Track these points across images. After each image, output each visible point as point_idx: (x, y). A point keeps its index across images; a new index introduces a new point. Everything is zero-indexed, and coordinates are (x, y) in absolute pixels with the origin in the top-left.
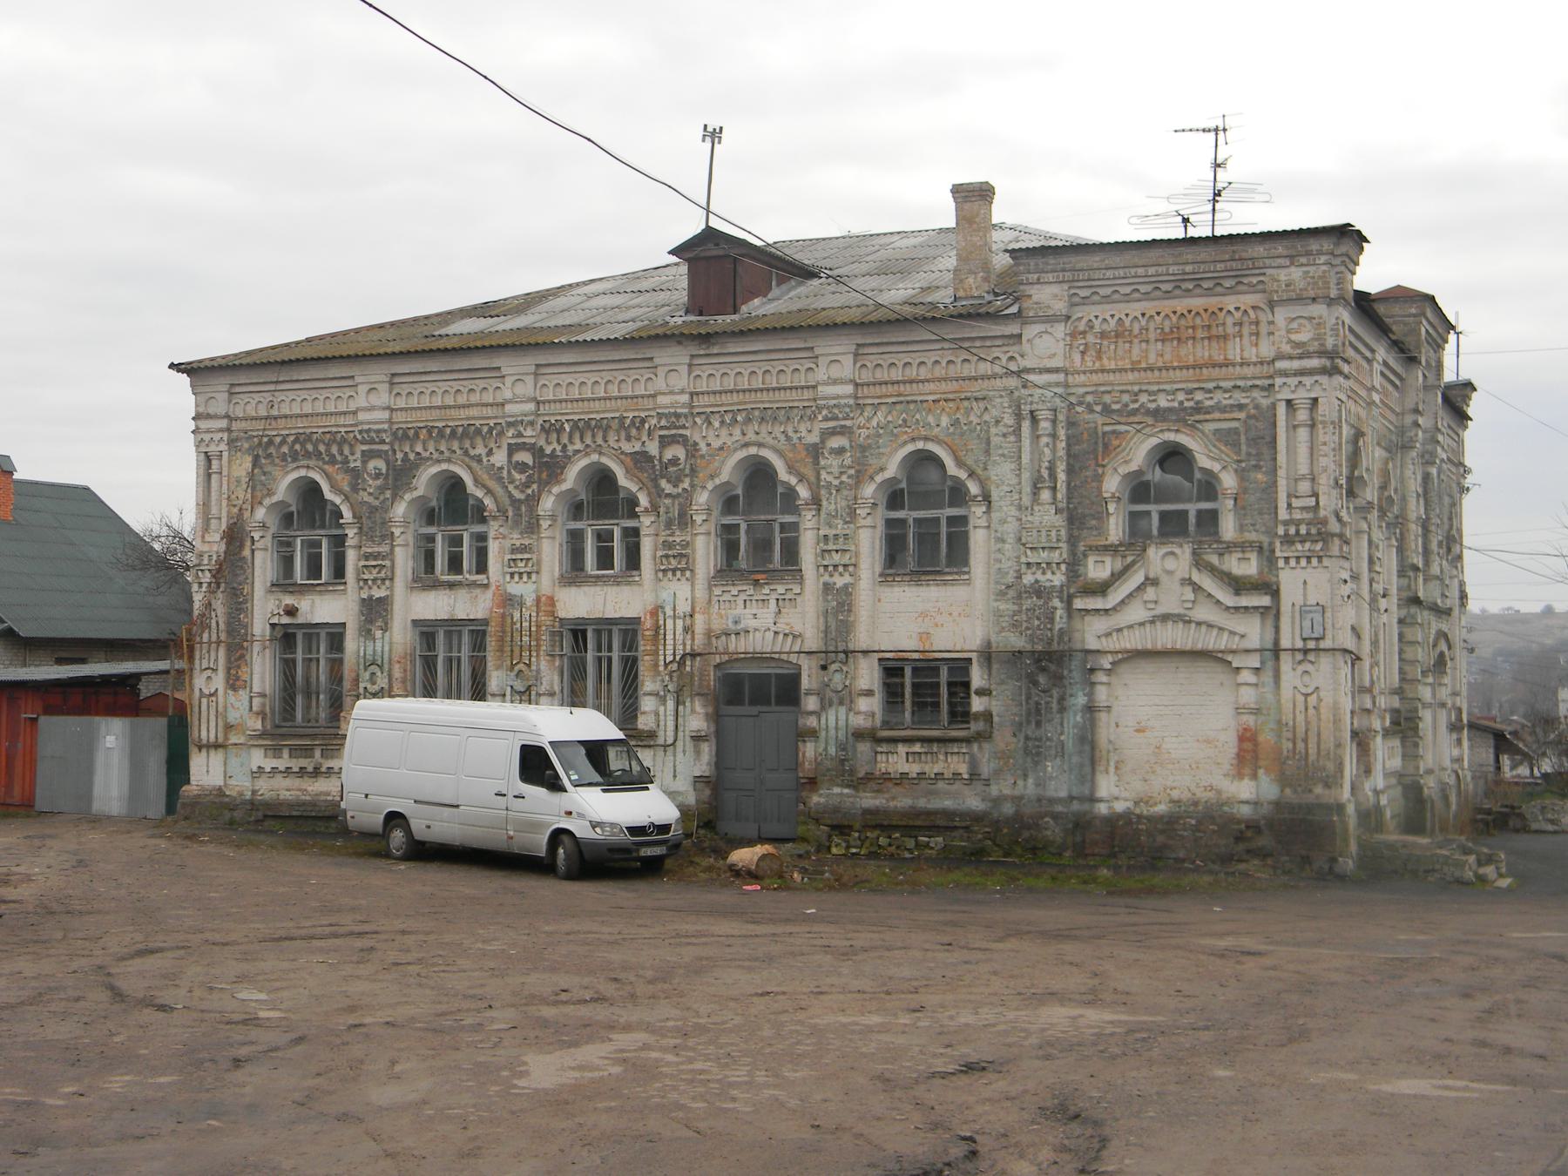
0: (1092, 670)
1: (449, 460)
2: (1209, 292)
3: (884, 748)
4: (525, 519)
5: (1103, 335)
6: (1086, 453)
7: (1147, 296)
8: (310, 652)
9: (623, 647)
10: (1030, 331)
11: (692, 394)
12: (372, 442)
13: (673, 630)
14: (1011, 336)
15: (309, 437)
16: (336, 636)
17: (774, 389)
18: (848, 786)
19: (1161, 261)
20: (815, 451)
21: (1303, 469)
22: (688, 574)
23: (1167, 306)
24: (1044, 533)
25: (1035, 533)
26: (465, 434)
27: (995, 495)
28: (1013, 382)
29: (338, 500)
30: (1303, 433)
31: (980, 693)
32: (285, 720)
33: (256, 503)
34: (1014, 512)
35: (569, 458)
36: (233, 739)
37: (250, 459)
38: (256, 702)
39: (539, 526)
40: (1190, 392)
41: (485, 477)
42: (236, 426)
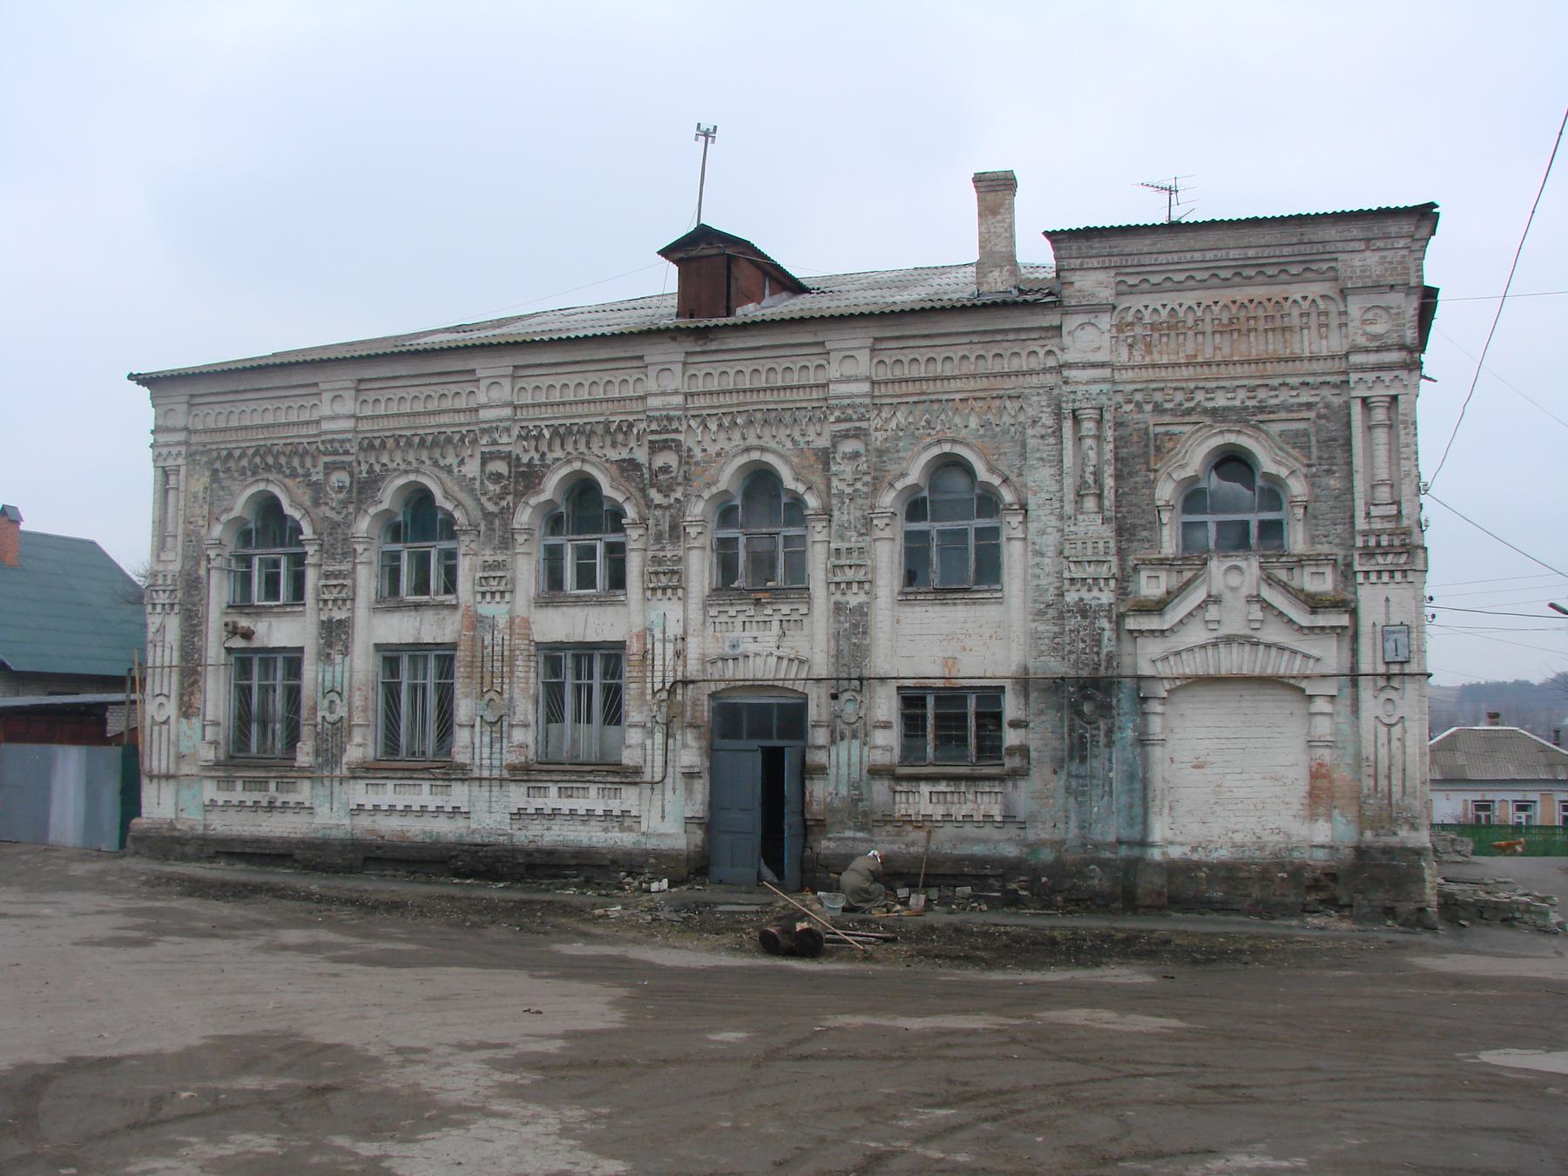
0: (1145, 699)
1: (417, 471)
2: (1272, 280)
3: (904, 787)
4: (498, 533)
5: (1153, 327)
6: (1137, 455)
7: (1203, 285)
8: (267, 678)
9: (605, 674)
10: (1071, 323)
11: (686, 395)
12: (335, 453)
13: (663, 654)
14: (1051, 328)
15: (269, 451)
16: (293, 660)
17: (779, 389)
18: (861, 829)
19: (1221, 245)
20: (825, 457)
21: (1382, 473)
22: (680, 592)
23: (1225, 295)
24: (1090, 545)
25: (1079, 545)
26: (435, 443)
27: (1032, 504)
28: (1050, 379)
29: (297, 515)
30: (1381, 435)
31: (1015, 724)
32: (240, 750)
33: (212, 518)
34: (1054, 522)
35: (548, 467)
36: (185, 769)
37: (207, 473)
38: (209, 730)
39: (514, 540)
40: (1253, 389)
41: (456, 488)
42: (195, 439)
